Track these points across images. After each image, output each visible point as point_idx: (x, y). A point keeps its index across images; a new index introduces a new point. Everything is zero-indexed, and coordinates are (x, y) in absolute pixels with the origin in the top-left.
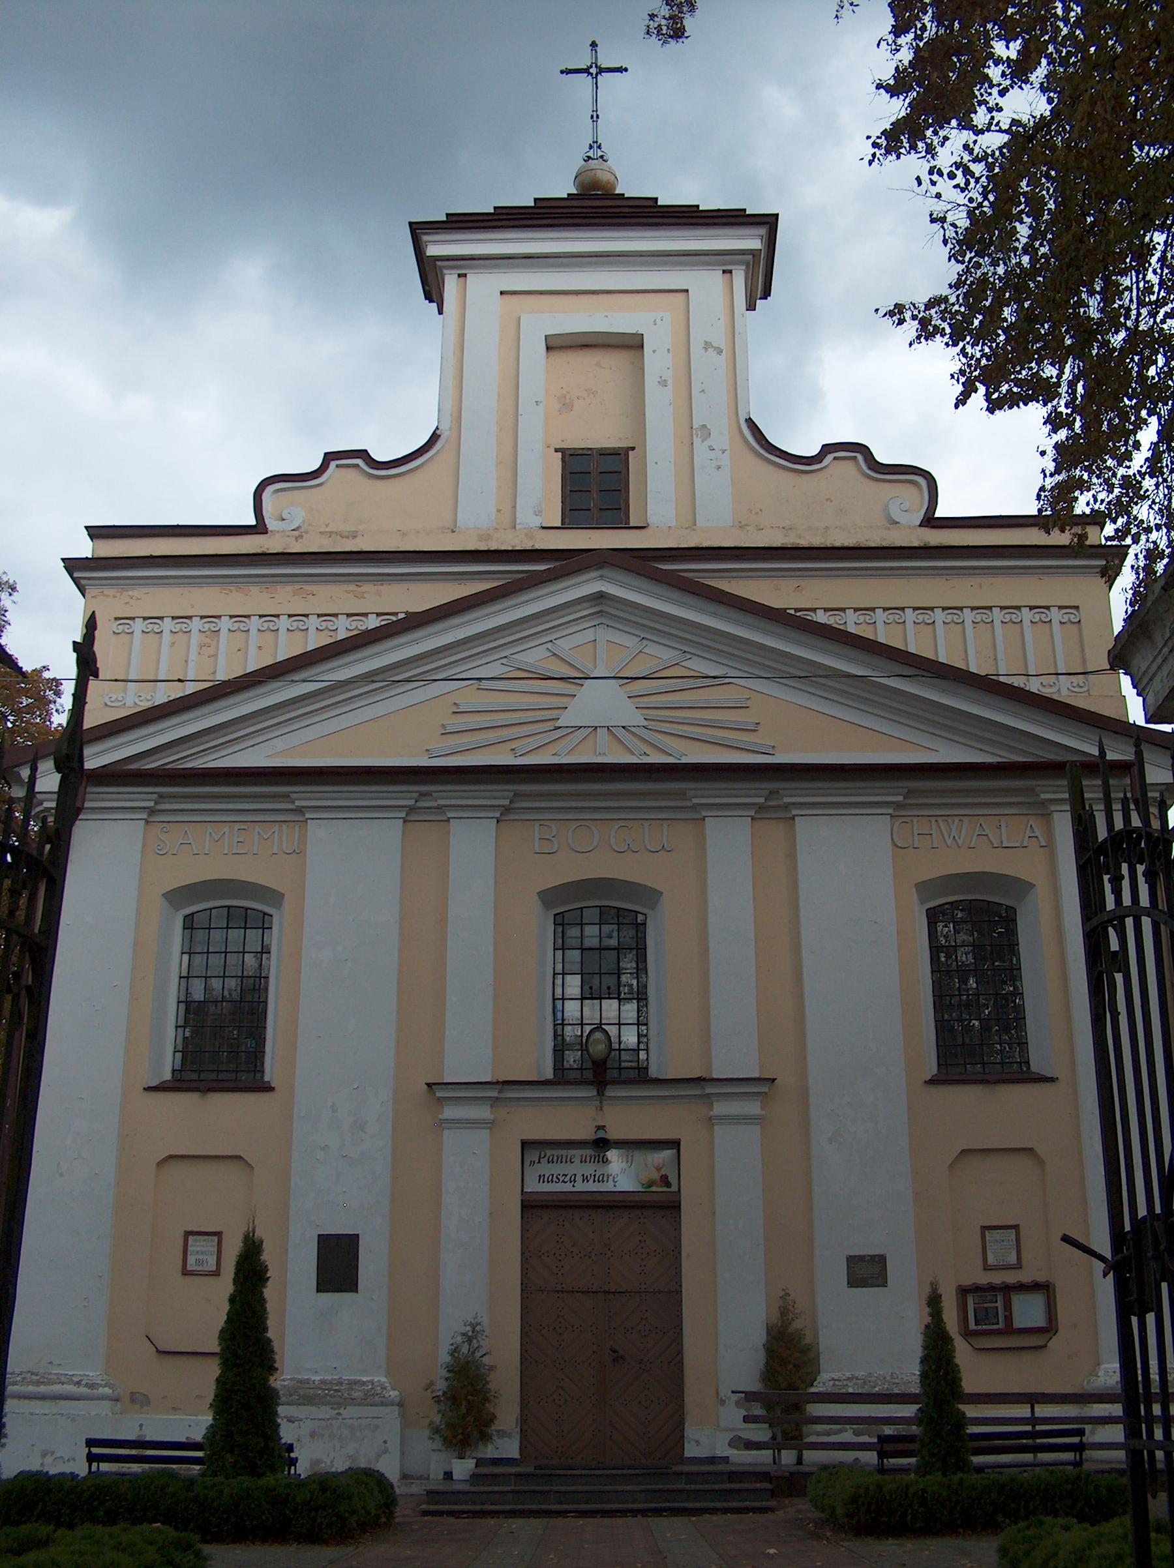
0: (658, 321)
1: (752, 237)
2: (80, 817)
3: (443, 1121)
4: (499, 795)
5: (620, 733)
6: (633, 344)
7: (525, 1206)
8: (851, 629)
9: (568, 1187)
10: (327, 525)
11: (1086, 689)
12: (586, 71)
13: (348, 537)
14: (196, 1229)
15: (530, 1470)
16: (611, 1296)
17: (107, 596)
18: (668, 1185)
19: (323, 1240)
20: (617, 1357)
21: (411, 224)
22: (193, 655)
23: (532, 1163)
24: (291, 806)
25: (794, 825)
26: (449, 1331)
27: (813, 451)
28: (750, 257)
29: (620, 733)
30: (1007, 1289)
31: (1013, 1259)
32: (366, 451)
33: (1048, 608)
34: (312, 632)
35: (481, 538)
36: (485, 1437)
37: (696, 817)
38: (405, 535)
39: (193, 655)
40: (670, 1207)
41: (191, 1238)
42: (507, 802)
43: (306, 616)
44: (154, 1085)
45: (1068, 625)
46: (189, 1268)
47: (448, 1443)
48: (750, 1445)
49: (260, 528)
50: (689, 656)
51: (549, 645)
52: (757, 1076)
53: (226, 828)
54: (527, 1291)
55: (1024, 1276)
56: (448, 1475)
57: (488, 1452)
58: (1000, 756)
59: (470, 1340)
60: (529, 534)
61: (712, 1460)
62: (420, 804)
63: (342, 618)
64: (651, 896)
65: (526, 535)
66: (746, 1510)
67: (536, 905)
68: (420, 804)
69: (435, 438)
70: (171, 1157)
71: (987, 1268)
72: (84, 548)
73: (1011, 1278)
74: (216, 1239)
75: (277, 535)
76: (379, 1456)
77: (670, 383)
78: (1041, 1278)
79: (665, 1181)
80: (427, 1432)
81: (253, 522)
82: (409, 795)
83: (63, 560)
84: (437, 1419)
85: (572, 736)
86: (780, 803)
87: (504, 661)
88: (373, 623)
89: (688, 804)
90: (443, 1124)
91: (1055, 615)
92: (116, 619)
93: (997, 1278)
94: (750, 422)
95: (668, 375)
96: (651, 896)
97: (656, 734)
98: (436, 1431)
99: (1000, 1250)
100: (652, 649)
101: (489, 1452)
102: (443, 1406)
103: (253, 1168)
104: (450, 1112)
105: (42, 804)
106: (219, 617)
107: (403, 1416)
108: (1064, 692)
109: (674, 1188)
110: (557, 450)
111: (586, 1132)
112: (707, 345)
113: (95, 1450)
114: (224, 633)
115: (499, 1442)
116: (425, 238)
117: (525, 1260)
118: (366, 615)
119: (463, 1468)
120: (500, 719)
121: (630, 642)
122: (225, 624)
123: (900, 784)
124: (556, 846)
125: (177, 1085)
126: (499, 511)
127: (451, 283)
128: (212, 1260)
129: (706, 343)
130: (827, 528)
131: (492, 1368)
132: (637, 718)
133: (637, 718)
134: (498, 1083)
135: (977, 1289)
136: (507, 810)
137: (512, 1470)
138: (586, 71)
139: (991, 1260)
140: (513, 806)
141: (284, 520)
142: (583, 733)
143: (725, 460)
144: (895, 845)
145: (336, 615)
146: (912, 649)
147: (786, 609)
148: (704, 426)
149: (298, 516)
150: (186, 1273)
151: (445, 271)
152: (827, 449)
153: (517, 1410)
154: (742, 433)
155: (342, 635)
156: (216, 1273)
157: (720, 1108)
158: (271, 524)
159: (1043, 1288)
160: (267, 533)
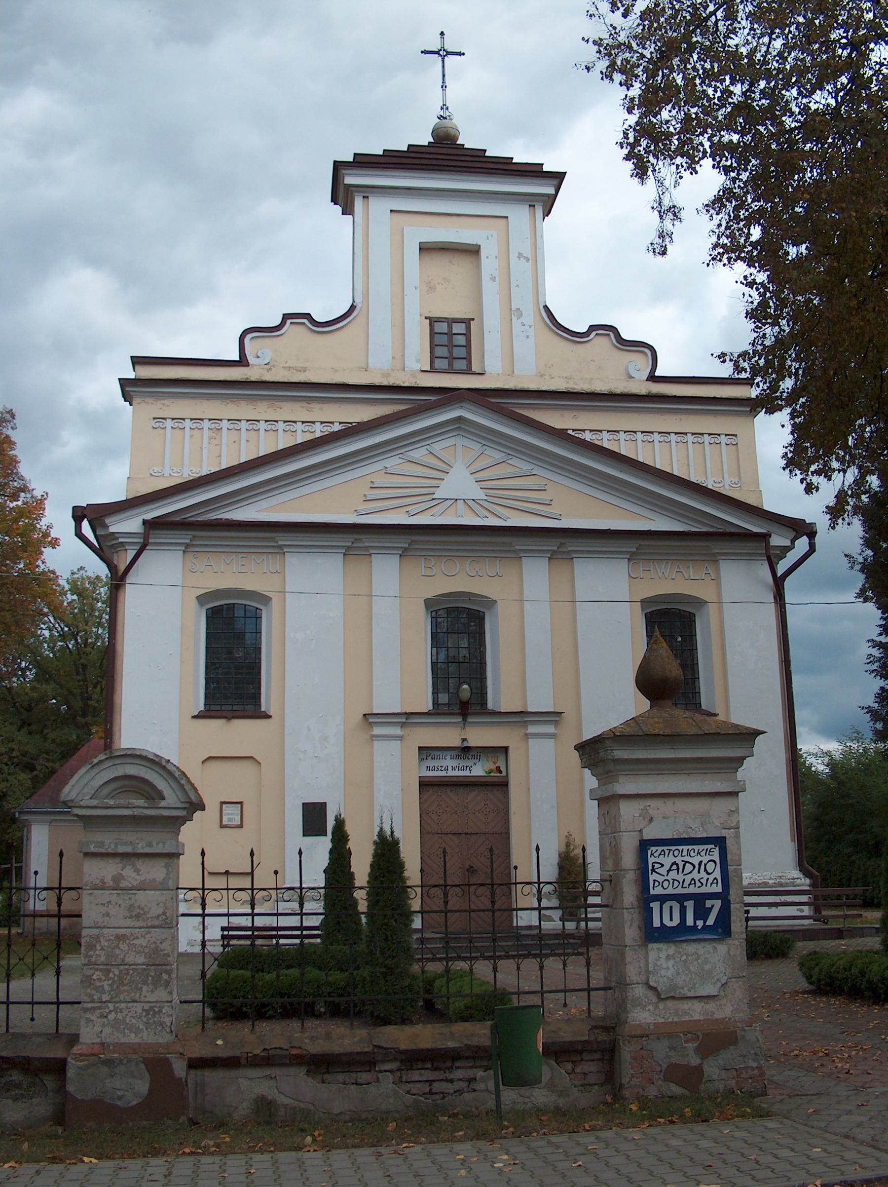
0: (490, 237)
1: (549, 185)
2: (147, 548)
4: (403, 542)
5: (471, 503)
6: (473, 251)
7: (420, 785)
8: (606, 445)
9: (444, 774)
10: (286, 362)
11: (739, 485)
13: (300, 371)
14: (227, 800)
16: (468, 836)
17: (148, 403)
18: (501, 772)
19: (305, 806)
22: (205, 444)
24: (276, 544)
25: (573, 563)
27: (583, 329)
28: (547, 198)
29: (471, 503)
32: (309, 314)
33: (719, 435)
34: (299, 432)
35: (386, 375)
37: (281, 550)
39: (205, 444)
40: (503, 785)
41: (224, 806)
42: (407, 545)
43: (276, 421)
44: (196, 714)
45: (730, 446)
46: (224, 823)
50: (511, 457)
51: (427, 447)
52: (552, 710)
53: (234, 556)
58: (714, 527)
60: (413, 375)
62: (354, 545)
63: (299, 424)
65: (411, 375)
68: (354, 545)
69: (352, 308)
70: (210, 758)
74: (239, 806)
75: (255, 367)
77: (497, 279)
79: (499, 770)
82: (187, 537)
85: (442, 504)
86: (566, 550)
87: (400, 456)
88: (337, 427)
89: (512, 549)
90: (374, 737)
91: (723, 439)
92: (154, 418)
94: (546, 307)
95: (496, 274)
97: (493, 505)
100: (489, 452)
103: (260, 763)
104: (377, 731)
105: (117, 538)
106: (221, 420)
108: (727, 487)
110: (426, 318)
111: (457, 743)
112: (520, 255)
113: (226, 933)
114: (225, 430)
118: (332, 423)
121: (477, 447)
122: (225, 424)
123: (190, 533)
124: (435, 571)
125: (208, 714)
126: (393, 358)
127: (358, 203)
128: (238, 818)
129: (519, 254)
130: (592, 379)
132: (480, 495)
133: (480, 495)
134: (406, 713)
136: (405, 550)
138: (448, 53)
140: (411, 547)
141: (258, 357)
142: (449, 503)
143: (531, 332)
144: (629, 576)
145: (295, 422)
146: (641, 460)
147: (567, 430)
148: (519, 309)
150: (222, 826)
151: (355, 194)
152: (592, 328)
154: (542, 317)
155: (318, 434)
157: (532, 729)
158: (251, 359)
160: (249, 366)
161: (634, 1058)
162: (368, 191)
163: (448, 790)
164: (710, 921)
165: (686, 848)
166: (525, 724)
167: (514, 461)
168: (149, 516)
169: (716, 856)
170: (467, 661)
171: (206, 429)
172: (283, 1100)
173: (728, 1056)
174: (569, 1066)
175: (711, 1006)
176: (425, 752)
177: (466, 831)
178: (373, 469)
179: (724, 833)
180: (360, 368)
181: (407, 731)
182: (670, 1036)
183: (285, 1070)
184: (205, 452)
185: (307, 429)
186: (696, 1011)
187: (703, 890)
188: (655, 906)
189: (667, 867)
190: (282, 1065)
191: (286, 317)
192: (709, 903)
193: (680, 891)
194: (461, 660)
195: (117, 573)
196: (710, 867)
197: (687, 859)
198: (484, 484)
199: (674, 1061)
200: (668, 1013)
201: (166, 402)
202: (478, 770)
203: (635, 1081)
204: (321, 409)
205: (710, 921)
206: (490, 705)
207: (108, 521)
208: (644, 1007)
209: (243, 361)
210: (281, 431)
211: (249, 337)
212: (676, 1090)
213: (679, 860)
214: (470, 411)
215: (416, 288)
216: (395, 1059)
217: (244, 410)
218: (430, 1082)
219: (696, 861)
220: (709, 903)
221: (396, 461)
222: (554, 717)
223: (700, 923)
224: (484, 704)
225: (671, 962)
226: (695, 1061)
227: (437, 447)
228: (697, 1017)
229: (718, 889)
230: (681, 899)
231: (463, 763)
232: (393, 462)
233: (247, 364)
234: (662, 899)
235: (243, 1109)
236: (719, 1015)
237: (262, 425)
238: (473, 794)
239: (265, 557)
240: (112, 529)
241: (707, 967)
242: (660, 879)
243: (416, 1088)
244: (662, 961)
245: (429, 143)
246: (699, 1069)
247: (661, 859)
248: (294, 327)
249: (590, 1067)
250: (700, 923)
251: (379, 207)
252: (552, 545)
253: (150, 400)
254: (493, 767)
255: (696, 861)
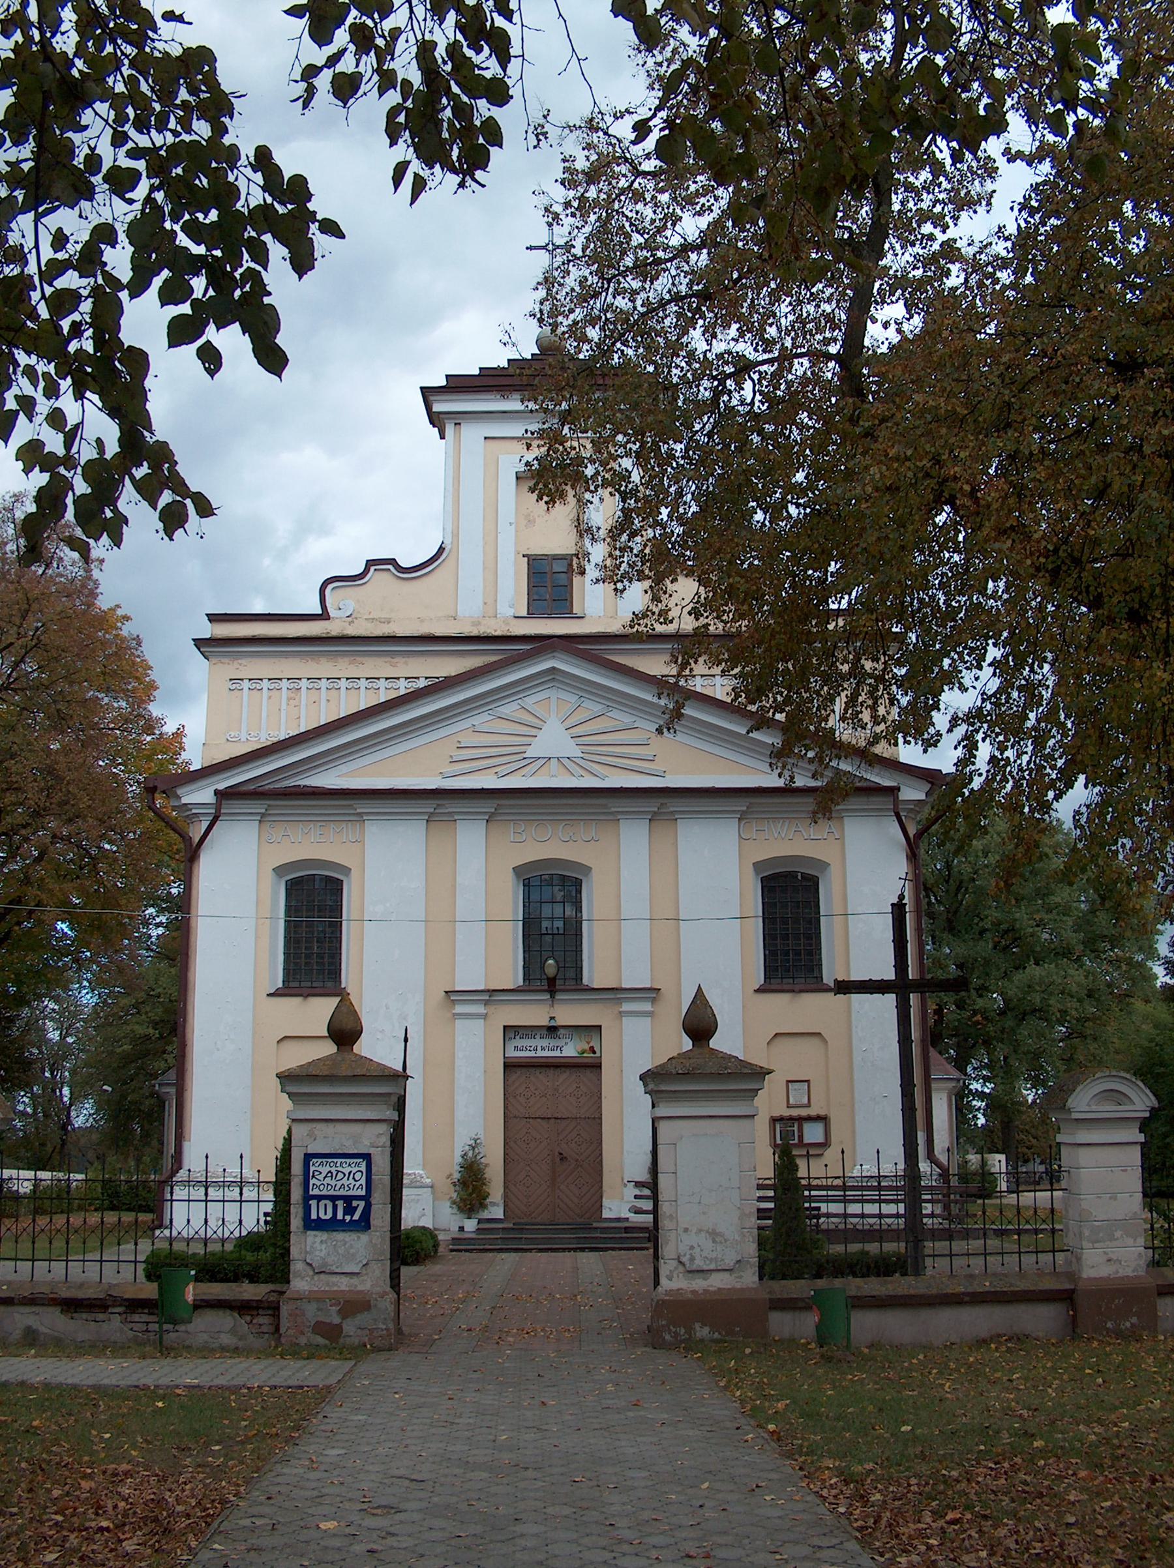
3: (454, 1014)
4: (489, 806)
7: (600, 1067)
9: (532, 1054)
12: (544, 248)
15: (511, 1225)
18: (594, 1052)
20: (563, 1159)
21: (422, 388)
22: (284, 706)
23: (510, 1039)
26: (461, 1145)
29: (566, 762)
30: (801, 1120)
31: (805, 1101)
35: (477, 624)
36: (483, 1206)
37: (360, 818)
38: (422, 621)
39: (284, 706)
47: (461, 1210)
48: (638, 1211)
49: (324, 616)
52: (648, 986)
54: (508, 1118)
55: (812, 1111)
56: (461, 1229)
57: (485, 1215)
59: (473, 1148)
60: (506, 622)
61: (618, 1220)
64: (587, 870)
66: (632, 1249)
67: (510, 875)
69: (441, 550)
70: (286, 1037)
71: (789, 1106)
72: (207, 630)
73: (804, 1112)
76: (420, 1218)
78: (822, 1113)
80: (448, 1204)
81: (320, 612)
83: (194, 640)
84: (455, 1195)
88: (422, 683)
93: (795, 1113)
96: (587, 870)
98: (454, 1203)
99: (798, 1095)
100: (587, 704)
101: (485, 1215)
102: (457, 1188)
104: (459, 1009)
107: (433, 1193)
109: (598, 1054)
111: (544, 1022)
114: (304, 689)
115: (492, 1209)
116: (432, 398)
117: (505, 1099)
119: (471, 1225)
120: (494, 751)
121: (573, 699)
122: (304, 684)
125: (287, 991)
131: (486, 1165)
132: (576, 752)
133: (576, 752)
134: (488, 991)
135: (781, 1119)
136: (492, 815)
137: (500, 1226)
138: (544, 248)
139: (792, 1101)
149: (349, 606)
153: (502, 1190)
155: (402, 692)
156: (789, 1106)
157: (626, 1007)
158: (332, 612)
159: (823, 1119)
161: (290, 1315)
162: (459, 418)
163: (538, 1071)
164: (356, 1217)
165: (339, 1161)
166: (620, 1001)
167: (615, 714)
168: (221, 786)
169: (363, 1168)
170: (561, 931)
171: (284, 689)
172: (43, 1329)
173: (363, 1319)
174: (248, 1318)
175: (355, 1281)
176: (510, 1031)
177: (556, 1115)
178: (461, 730)
179: (371, 1151)
180: (448, 617)
181: (491, 1009)
182: (318, 1300)
183: (45, 1308)
184: (283, 713)
185: (390, 685)
186: (343, 1284)
187: (351, 1193)
188: (313, 1203)
189: (324, 1175)
190: (43, 1305)
191: (370, 563)
192: (355, 1203)
193: (332, 1193)
194: (555, 931)
195: (191, 845)
196: (358, 1176)
197: (340, 1169)
198: (580, 741)
199: (320, 1319)
200: (321, 1284)
201: (243, 661)
202: (570, 1049)
203: (291, 1332)
204: (406, 663)
205: (356, 1217)
206: (585, 981)
207: (180, 792)
208: (302, 1278)
209: (324, 616)
210: (363, 689)
211: (330, 587)
212: (320, 1340)
213: (333, 1170)
214: (563, 661)
215: (511, 524)
216: (120, 1305)
217: (324, 668)
218: (147, 1323)
219: (346, 1171)
220: (355, 1203)
221: (485, 717)
222: (652, 993)
223: (348, 1218)
224: (579, 977)
225: (324, 1246)
226: (336, 1320)
227: (529, 702)
228: (343, 1288)
229: (363, 1193)
230: (333, 1199)
231: (553, 1043)
232: (480, 720)
233: (328, 618)
234: (319, 1198)
235: (17, 1334)
236: (360, 1288)
237: (343, 684)
238: (564, 1076)
239: (344, 825)
240: (184, 800)
241: (352, 1251)
242: (318, 1183)
243: (137, 1327)
244: (317, 1245)
245: (533, 355)
246: (339, 1327)
247: (320, 1169)
248: (378, 574)
249: (264, 1320)
250: (348, 1218)
251: (473, 434)
252: (652, 806)
253: (226, 660)
254: (587, 1047)
255: (346, 1171)
